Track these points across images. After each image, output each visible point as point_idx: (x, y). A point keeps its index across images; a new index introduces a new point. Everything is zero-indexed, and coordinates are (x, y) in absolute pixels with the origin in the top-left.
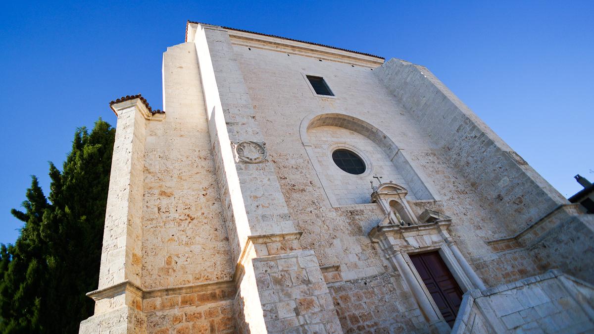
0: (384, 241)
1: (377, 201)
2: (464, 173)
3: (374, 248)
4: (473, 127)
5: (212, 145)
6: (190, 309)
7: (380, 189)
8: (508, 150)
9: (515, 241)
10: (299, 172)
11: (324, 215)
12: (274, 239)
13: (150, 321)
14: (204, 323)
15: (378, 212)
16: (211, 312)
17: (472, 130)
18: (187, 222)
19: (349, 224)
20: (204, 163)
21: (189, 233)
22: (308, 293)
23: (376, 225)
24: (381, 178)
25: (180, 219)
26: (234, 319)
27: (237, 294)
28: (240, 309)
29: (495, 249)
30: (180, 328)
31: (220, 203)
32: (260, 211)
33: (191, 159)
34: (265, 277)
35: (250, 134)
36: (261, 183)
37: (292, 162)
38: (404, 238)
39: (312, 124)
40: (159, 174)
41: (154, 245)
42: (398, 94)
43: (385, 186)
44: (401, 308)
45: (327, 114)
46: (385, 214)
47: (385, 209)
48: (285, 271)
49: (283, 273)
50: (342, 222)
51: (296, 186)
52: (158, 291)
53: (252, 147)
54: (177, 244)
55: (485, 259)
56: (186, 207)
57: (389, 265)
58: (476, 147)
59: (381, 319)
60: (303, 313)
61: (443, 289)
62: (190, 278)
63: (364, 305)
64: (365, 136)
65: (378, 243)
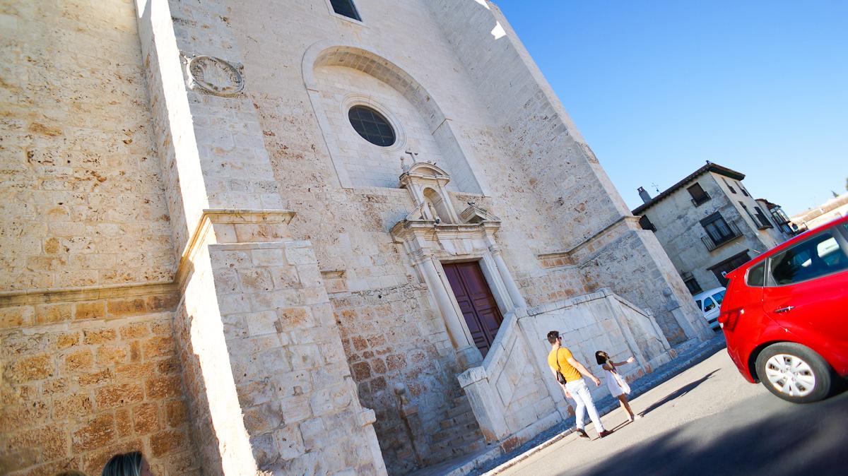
0: (410, 242)
1: (407, 186)
2: (524, 165)
3: (396, 251)
4: (545, 104)
5: (145, 58)
6: (91, 325)
7: (414, 169)
8: (581, 141)
9: (568, 256)
10: (295, 129)
11: (328, 196)
12: (247, 218)
13: (8, 344)
14: (121, 346)
15: (407, 201)
16: (133, 329)
17: (543, 108)
18: (91, 183)
19: (365, 214)
20: (126, 87)
21: (95, 202)
22: (298, 301)
23: (402, 219)
24: (416, 154)
25: (76, 178)
26: (175, 340)
27: (181, 302)
28: (185, 325)
29: (546, 264)
30: (74, 354)
31: (155, 159)
32: (227, 174)
33: (100, 76)
34: (230, 274)
35: (217, 44)
36: (231, 129)
37: (286, 112)
38: (438, 240)
39: (323, 58)
40: (28, 91)
41: (19, 218)
42: (454, 40)
43: (421, 166)
44: (425, 331)
45: (348, 47)
46: (416, 205)
47: (416, 198)
48: (264, 267)
49: (259, 270)
50: (354, 209)
51: (289, 149)
52: (28, 295)
53: (219, 68)
54: (69, 218)
55: (532, 275)
56: (90, 158)
57: (415, 275)
58: (544, 131)
59: (396, 344)
60: (286, 329)
61: (478, 309)
62: (96, 275)
63: (375, 325)
64: (400, 92)
65: (402, 243)
